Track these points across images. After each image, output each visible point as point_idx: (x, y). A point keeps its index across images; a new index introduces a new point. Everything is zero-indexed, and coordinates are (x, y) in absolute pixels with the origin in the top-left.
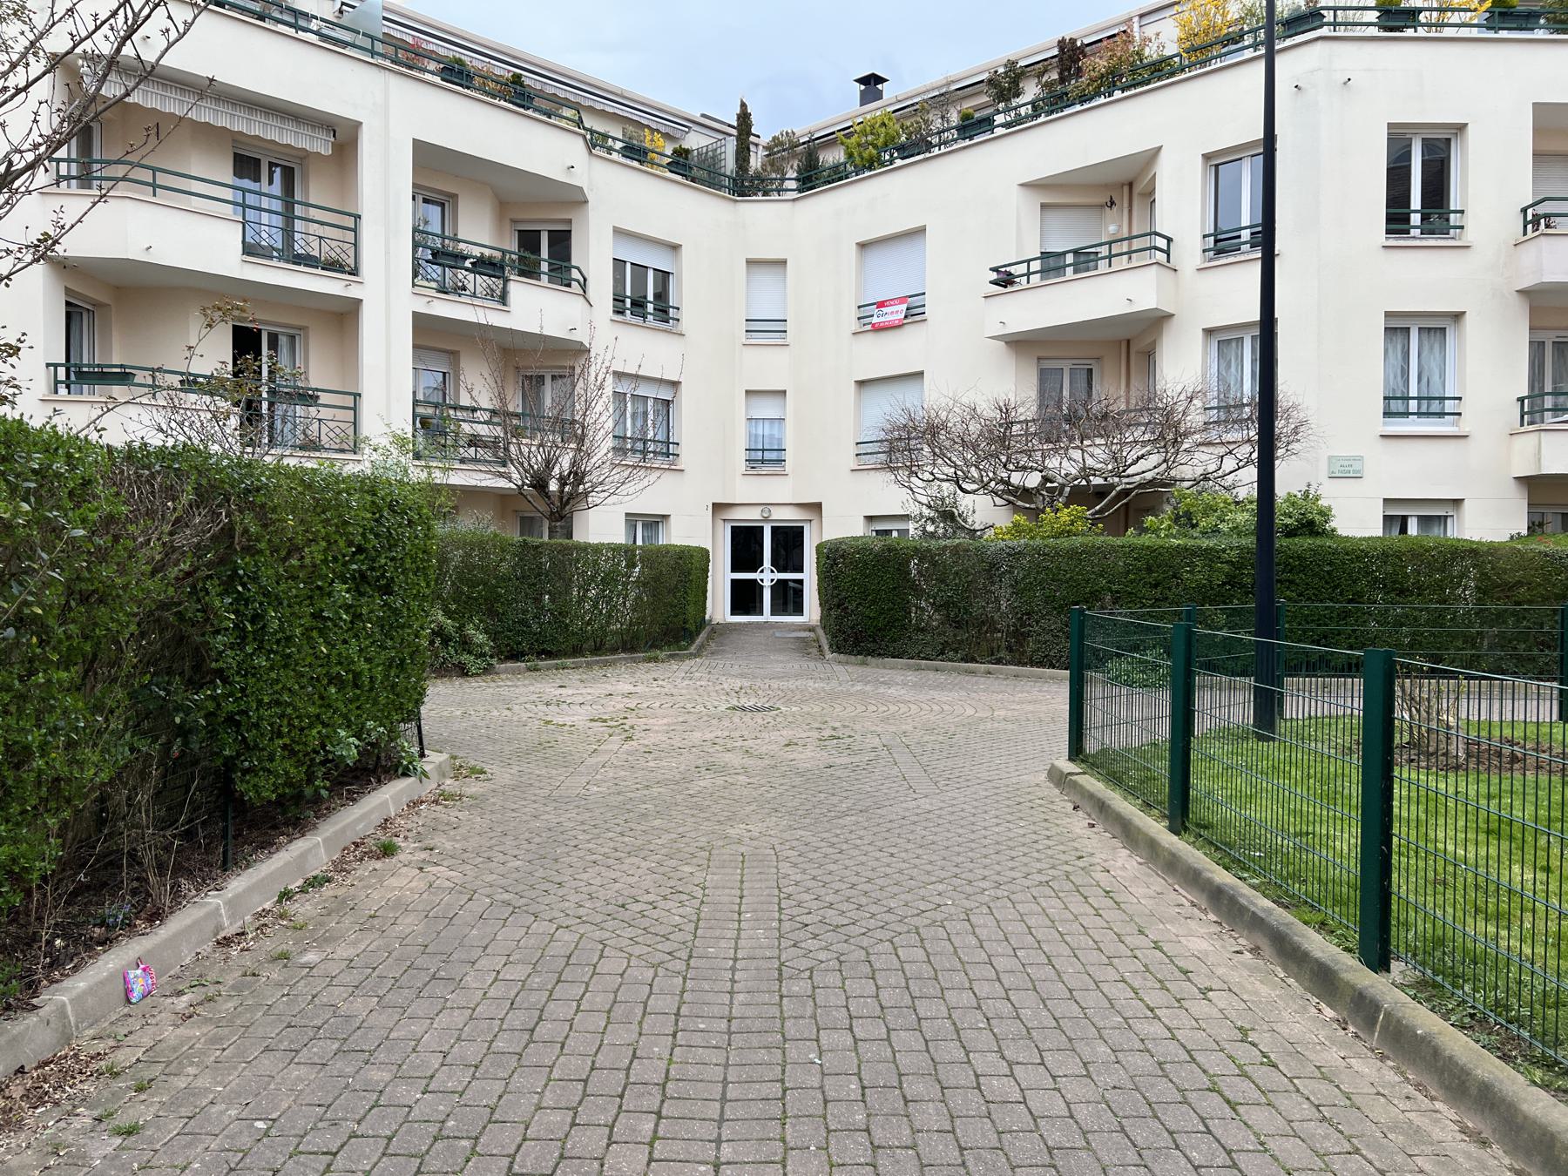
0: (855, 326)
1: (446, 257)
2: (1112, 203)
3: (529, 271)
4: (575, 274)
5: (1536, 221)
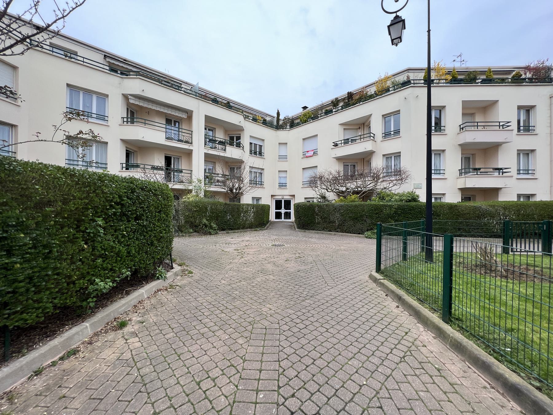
0: (302, 156)
1: (213, 141)
2: (360, 128)
3: (231, 144)
4: (241, 145)
5: (463, 128)
